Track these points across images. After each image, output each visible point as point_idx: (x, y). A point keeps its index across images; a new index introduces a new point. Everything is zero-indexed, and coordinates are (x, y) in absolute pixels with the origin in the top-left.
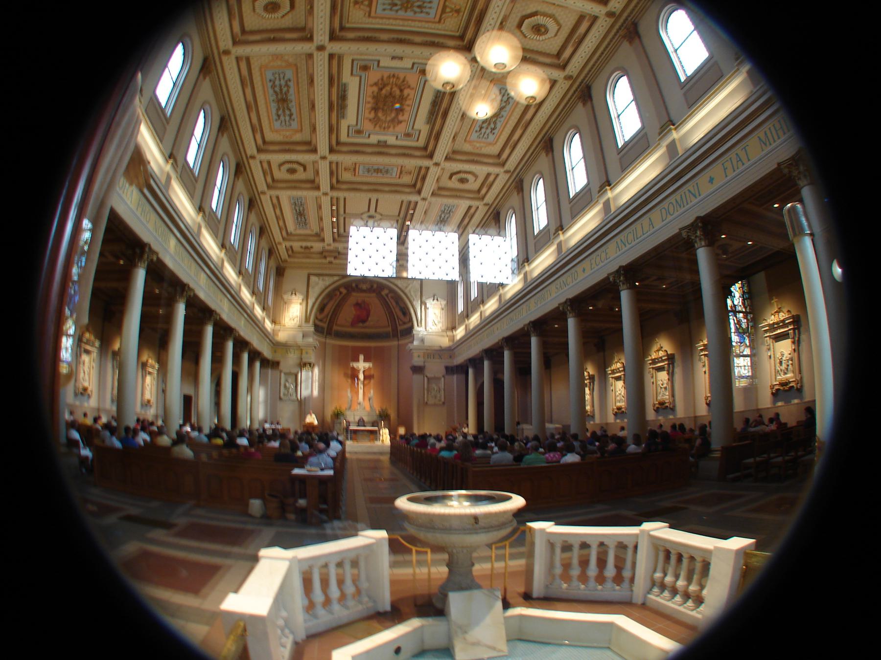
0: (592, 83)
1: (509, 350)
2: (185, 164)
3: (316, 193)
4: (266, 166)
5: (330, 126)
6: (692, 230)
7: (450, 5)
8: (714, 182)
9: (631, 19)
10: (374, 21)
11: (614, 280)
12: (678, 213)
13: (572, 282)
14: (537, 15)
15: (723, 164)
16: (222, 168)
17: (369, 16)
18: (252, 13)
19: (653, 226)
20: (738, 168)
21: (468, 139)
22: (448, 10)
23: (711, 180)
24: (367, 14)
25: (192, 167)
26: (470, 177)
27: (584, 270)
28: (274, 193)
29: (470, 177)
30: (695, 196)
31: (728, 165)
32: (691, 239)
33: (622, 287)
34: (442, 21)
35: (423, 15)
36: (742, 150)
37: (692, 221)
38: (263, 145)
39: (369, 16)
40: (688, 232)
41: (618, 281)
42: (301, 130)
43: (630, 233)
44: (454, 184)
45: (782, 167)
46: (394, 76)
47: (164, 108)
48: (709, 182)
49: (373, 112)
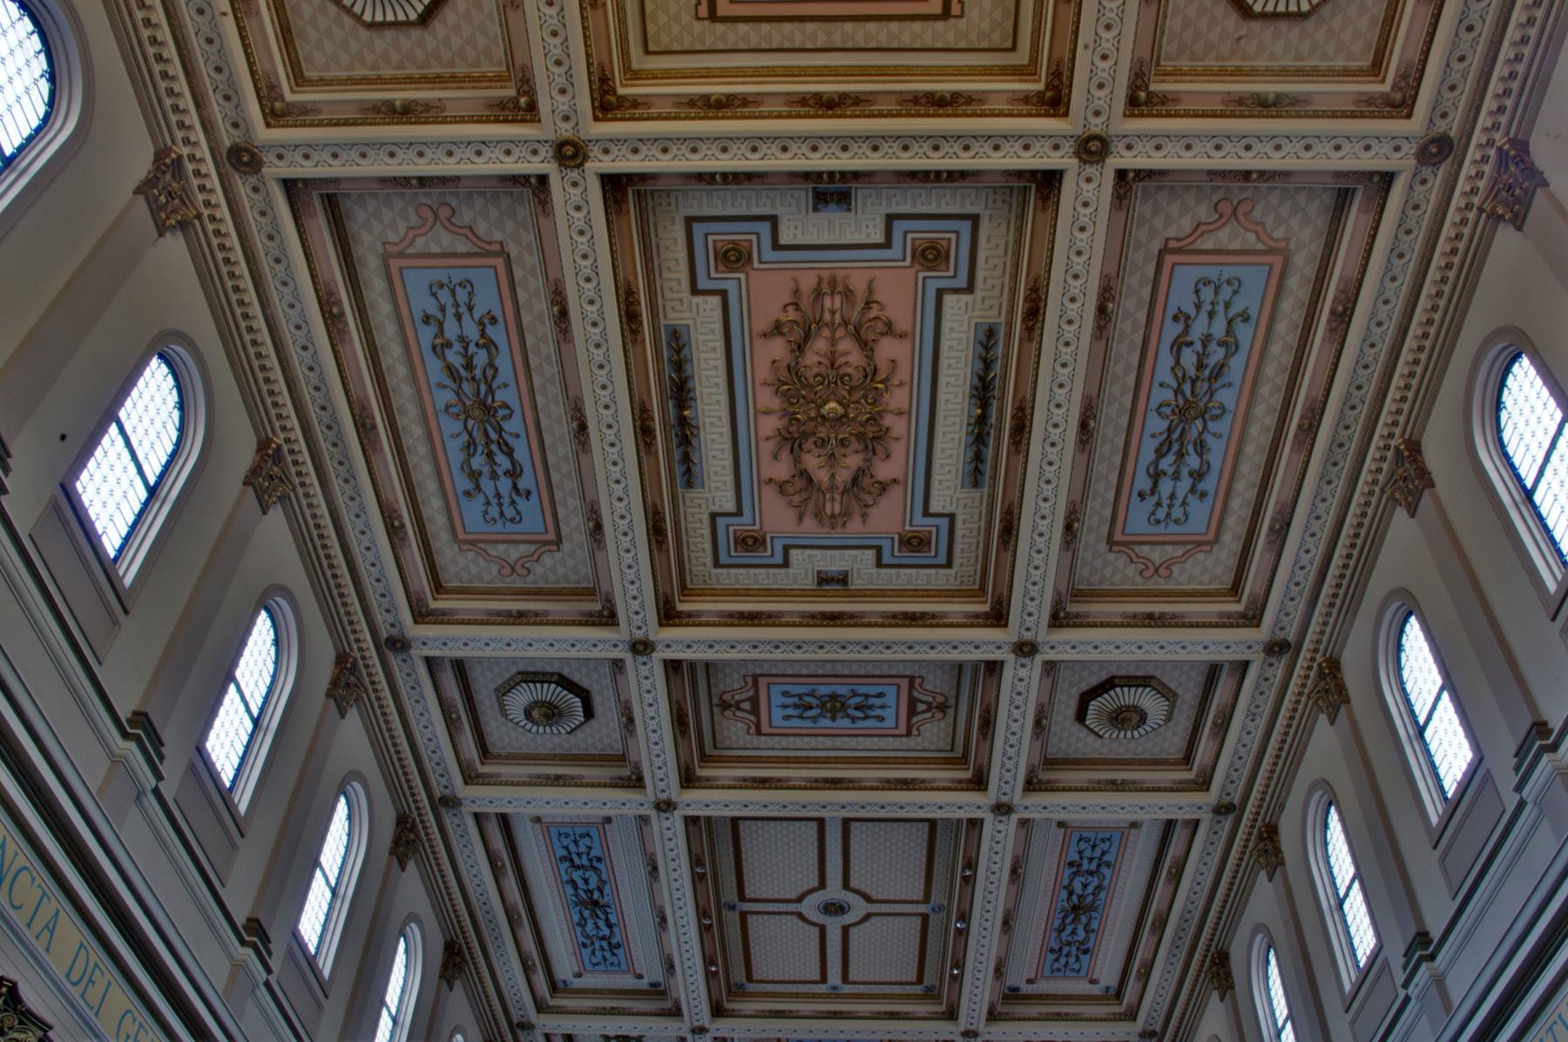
0: (1421, 435)
7: (924, 698)
9: (1264, 819)
10: (770, 741)
14: (1113, 688)
16: (403, 970)
17: (759, 732)
18: (502, 720)
21: (1118, 537)
22: (921, 707)
24: (753, 730)
25: (313, 951)
26: (1149, 701)
29: (1149, 701)
34: (915, 732)
35: (871, 723)
38: (482, 763)
39: (759, 732)
42: (558, 541)
46: (833, 283)
47: (228, 784)
49: (785, 455)
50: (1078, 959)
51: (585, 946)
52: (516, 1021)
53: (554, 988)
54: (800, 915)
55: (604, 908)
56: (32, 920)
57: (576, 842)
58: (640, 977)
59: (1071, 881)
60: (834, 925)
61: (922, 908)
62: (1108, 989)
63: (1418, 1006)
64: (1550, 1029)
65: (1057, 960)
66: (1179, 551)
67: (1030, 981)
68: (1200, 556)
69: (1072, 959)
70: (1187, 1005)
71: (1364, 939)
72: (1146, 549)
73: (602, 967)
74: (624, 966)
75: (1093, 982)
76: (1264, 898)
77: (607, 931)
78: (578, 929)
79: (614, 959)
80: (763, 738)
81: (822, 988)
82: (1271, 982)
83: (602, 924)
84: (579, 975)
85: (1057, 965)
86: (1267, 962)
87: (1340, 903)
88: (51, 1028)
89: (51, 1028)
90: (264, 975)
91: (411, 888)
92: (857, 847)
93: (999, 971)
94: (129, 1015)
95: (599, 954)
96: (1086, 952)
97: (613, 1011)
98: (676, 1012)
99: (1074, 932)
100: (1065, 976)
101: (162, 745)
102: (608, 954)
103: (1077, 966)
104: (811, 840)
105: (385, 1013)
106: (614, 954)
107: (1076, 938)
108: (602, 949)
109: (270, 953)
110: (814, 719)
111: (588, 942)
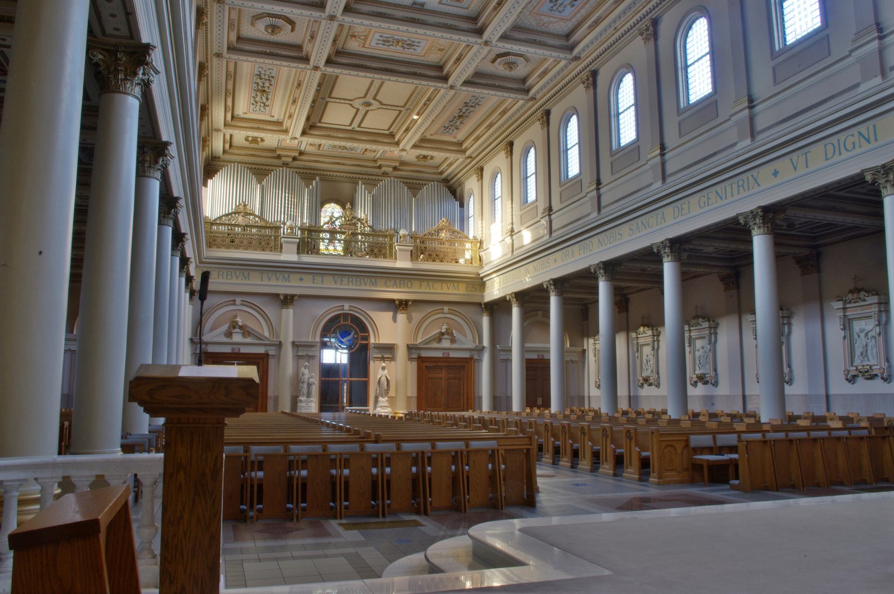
1: (606, 280)
6: (882, 173)
8: (778, 175)
11: (746, 221)
15: (825, 146)
23: (776, 173)
27: (555, 260)
30: (868, 141)
31: (830, 148)
32: (877, 182)
33: (665, 259)
36: (802, 155)
40: (873, 174)
41: (662, 252)
43: (704, 196)
44: (499, 68)
45: (653, 247)
48: (773, 174)
51: (253, 104)
56: (792, 161)
59: (463, 108)
61: (329, 100)
62: (459, 141)
64: (732, 184)
66: (555, 20)
68: (562, 23)
72: (543, 17)
74: (267, 112)
78: (252, 99)
79: (264, 110)
84: (246, 113)
96: (457, 129)
97: (258, 129)
106: (265, 109)
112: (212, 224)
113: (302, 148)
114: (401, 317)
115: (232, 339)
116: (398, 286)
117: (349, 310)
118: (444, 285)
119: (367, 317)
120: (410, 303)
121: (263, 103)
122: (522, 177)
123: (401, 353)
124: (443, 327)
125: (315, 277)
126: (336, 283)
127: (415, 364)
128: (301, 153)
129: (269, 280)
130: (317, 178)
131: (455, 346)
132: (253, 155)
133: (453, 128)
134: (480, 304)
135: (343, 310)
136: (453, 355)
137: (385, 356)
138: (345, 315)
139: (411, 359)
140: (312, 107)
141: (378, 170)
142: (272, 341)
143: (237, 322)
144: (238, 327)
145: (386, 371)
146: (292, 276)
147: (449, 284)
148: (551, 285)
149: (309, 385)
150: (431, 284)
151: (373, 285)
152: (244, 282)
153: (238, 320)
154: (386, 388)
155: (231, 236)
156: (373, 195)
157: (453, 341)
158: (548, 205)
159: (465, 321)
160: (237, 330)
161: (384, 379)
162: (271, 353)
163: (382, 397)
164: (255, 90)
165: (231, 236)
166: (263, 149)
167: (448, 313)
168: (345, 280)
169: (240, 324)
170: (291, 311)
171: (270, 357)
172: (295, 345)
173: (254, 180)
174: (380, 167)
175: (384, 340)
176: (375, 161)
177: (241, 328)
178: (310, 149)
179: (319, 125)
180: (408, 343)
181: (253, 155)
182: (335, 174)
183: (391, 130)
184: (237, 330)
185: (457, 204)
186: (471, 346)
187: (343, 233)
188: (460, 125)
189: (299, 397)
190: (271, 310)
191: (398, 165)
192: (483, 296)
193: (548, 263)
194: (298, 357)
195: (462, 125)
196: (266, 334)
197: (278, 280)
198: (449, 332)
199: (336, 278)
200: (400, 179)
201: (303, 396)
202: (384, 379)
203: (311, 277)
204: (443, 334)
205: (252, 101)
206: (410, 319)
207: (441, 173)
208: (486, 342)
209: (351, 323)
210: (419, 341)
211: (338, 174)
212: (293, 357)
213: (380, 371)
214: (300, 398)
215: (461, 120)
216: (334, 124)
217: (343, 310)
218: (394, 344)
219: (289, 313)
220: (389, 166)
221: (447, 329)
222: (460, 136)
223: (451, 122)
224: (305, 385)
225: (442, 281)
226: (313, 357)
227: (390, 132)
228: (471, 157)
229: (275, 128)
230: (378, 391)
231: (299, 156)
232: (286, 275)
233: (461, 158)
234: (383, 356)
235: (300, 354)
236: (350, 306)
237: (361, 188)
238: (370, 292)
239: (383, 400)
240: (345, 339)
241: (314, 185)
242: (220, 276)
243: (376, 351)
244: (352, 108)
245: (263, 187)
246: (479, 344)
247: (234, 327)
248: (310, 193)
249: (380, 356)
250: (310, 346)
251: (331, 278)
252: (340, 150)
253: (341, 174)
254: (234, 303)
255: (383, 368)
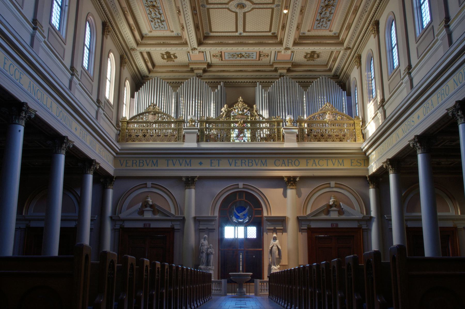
2: (51, 28)
3: (185, 49)
4: (146, 56)
5: (196, 25)
9: (357, 53)
12: (428, 114)
13: (411, 128)
17: (222, 60)
19: (433, 106)
20: (431, 110)
22: (262, 56)
24: (221, 60)
28: (145, 49)
34: (260, 60)
37: (454, 105)
50: (326, 23)
51: (152, 21)
52: (130, 48)
53: (142, 37)
54: (228, 9)
55: (157, 7)
57: (160, 26)
58: (173, 32)
60: (240, 12)
61: (208, 6)
62: (335, 34)
63: (441, 41)
65: (319, 23)
67: (308, 31)
69: (324, 23)
70: (349, 66)
71: (427, 19)
73: (158, 29)
74: (166, 28)
75: (330, 31)
76: (372, 43)
77: (159, 16)
79: (162, 26)
80: (223, 61)
81: (237, 34)
82: (392, 32)
83: (157, 13)
84: (151, 32)
85: (318, 25)
86: (392, 25)
87: (421, 5)
88: (36, 111)
89: (36, 111)
90: (43, 39)
91: (109, 42)
92: (248, 16)
93: (298, 28)
94: (17, 70)
95: (157, 24)
96: (329, 21)
98: (185, 44)
99: (325, 13)
100: (321, 29)
101: (77, 72)
102: (160, 24)
103: (326, 26)
104: (233, 20)
105: (107, 80)
106: (162, 24)
107: (326, 16)
108: (158, 22)
109: (43, 31)
110: (236, 58)
111: (153, 20)
112: (128, 123)
113: (209, 61)
114: (291, 192)
115: (143, 216)
116: (287, 165)
117: (243, 188)
118: (330, 162)
119: (259, 193)
120: (298, 179)
121: (158, 19)
122: (388, 49)
123: (292, 225)
124: (331, 200)
125: (212, 161)
126: (231, 165)
127: (305, 234)
128: (209, 65)
129: (174, 165)
130: (222, 83)
131: (343, 217)
132: (172, 71)
133: (325, 20)
134: (365, 178)
135: (238, 188)
136: (341, 225)
137: (277, 228)
138: (241, 192)
139: (301, 230)
140: (194, 14)
141: (274, 74)
142: (177, 217)
143: (147, 202)
144: (148, 206)
145: (277, 241)
146: (193, 161)
147: (334, 161)
148: (416, 142)
149: (208, 255)
150: (317, 161)
151: (264, 165)
152: (154, 168)
153: (149, 200)
154: (278, 257)
155: (144, 131)
156: (269, 93)
157: (341, 212)
158: (407, 64)
159: (352, 194)
160: (148, 208)
161: (275, 248)
162: (176, 227)
163: (274, 265)
164: (147, 7)
165: (144, 131)
166: (177, 66)
167: (335, 187)
168: (239, 162)
169: (151, 203)
170: (193, 191)
171: (176, 231)
172: (196, 219)
173: (170, 88)
174: (276, 70)
175: (274, 214)
176: (272, 66)
177: (151, 206)
178: (216, 61)
179: (212, 34)
180: (298, 215)
181: (172, 71)
182: (240, 81)
183: (272, 31)
184: (148, 208)
185: (344, 93)
186: (358, 216)
187: (237, 122)
188: (330, 16)
189: (199, 265)
190: (176, 192)
191: (290, 66)
192: (368, 170)
193: (413, 121)
194: (199, 231)
195: (332, 15)
196: (173, 212)
197: (181, 165)
198: (336, 204)
199: (231, 161)
200: (296, 80)
201: (203, 265)
202: (275, 248)
203: (209, 161)
204: (331, 206)
205: (150, 19)
206: (299, 194)
207: (330, 70)
208: (373, 213)
209: (246, 199)
210: (309, 212)
211: (243, 80)
212: (195, 231)
213: (272, 241)
214: (200, 266)
215: (329, 9)
216: (220, 32)
217: (238, 188)
218: (285, 217)
219: (192, 193)
220: (283, 68)
221: (334, 202)
222: (335, 28)
223: (321, 14)
224: (204, 255)
225: (327, 158)
226: (212, 230)
227: (272, 34)
228: (349, 48)
229: (177, 42)
230: (271, 260)
231: (208, 68)
232: (188, 161)
233: (341, 49)
234: (275, 228)
235: (201, 227)
236: (244, 184)
237: (259, 87)
238: (259, 172)
239: (275, 268)
240: (241, 214)
241: (219, 89)
242: (134, 165)
243: (269, 223)
244: (229, 12)
245: (177, 94)
246: (367, 214)
247: (146, 206)
248: (216, 95)
249: (273, 228)
250: (209, 220)
251: (226, 161)
252: (239, 58)
253: (246, 81)
254: (145, 186)
255: (275, 239)
